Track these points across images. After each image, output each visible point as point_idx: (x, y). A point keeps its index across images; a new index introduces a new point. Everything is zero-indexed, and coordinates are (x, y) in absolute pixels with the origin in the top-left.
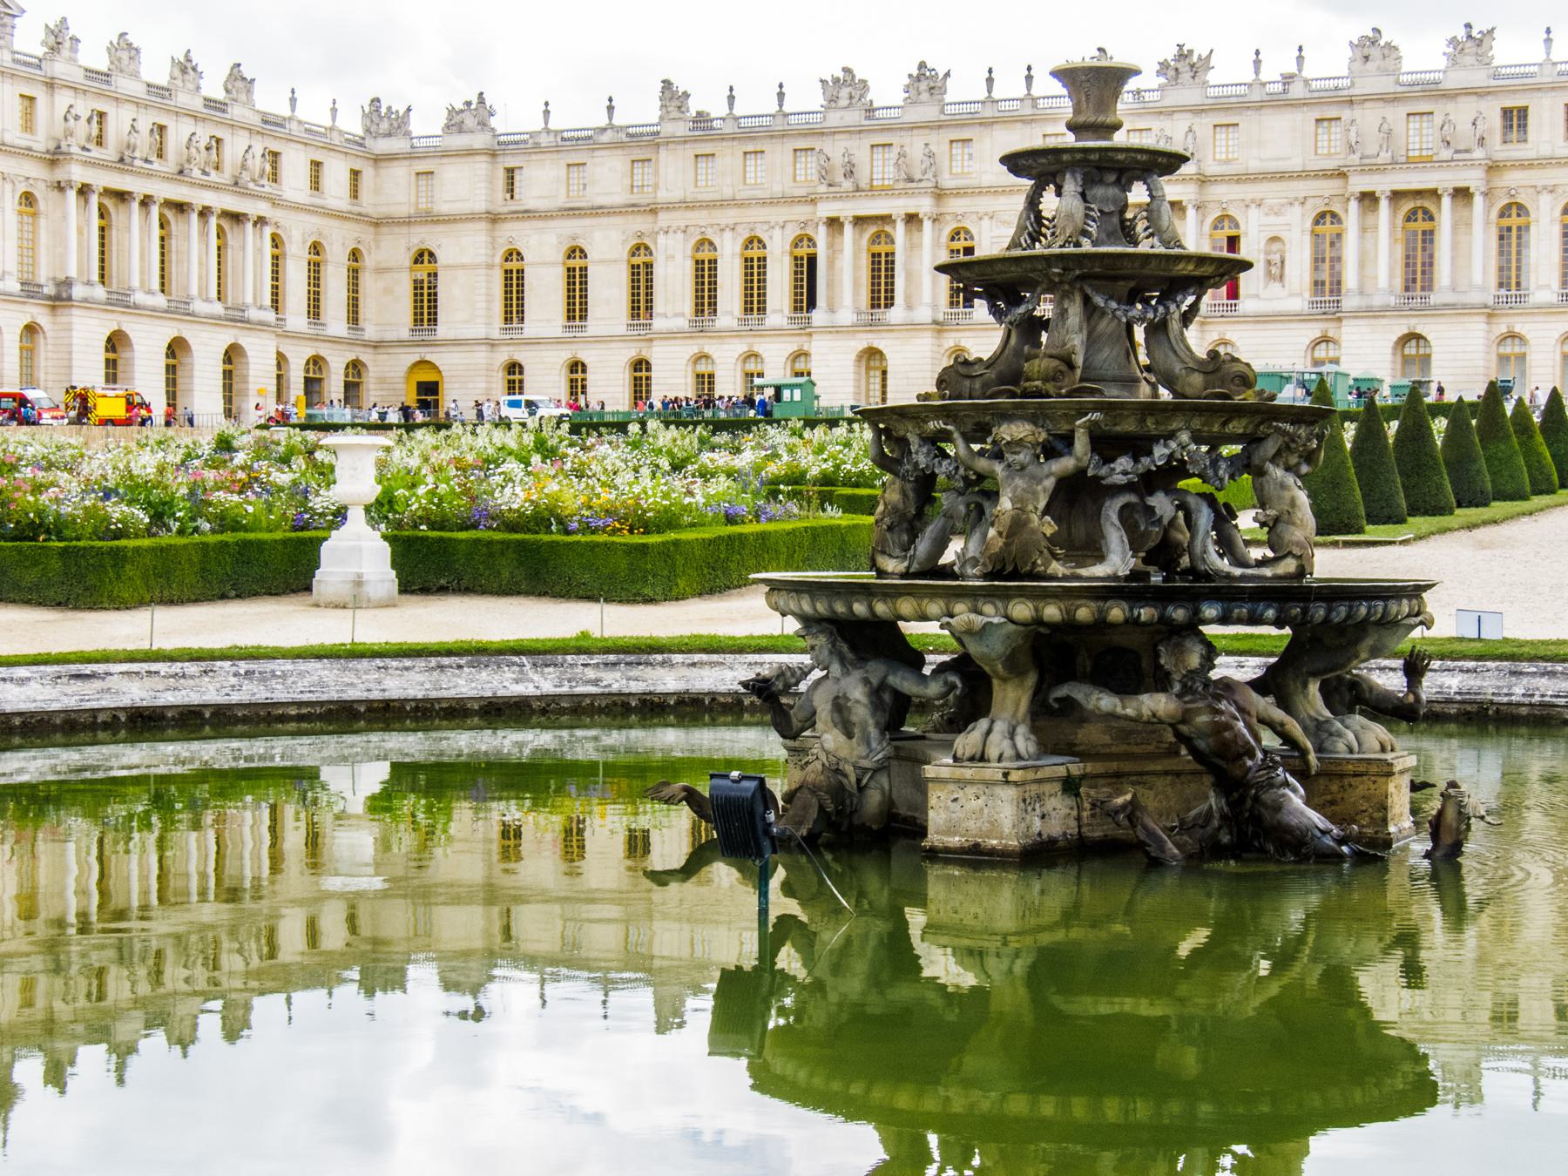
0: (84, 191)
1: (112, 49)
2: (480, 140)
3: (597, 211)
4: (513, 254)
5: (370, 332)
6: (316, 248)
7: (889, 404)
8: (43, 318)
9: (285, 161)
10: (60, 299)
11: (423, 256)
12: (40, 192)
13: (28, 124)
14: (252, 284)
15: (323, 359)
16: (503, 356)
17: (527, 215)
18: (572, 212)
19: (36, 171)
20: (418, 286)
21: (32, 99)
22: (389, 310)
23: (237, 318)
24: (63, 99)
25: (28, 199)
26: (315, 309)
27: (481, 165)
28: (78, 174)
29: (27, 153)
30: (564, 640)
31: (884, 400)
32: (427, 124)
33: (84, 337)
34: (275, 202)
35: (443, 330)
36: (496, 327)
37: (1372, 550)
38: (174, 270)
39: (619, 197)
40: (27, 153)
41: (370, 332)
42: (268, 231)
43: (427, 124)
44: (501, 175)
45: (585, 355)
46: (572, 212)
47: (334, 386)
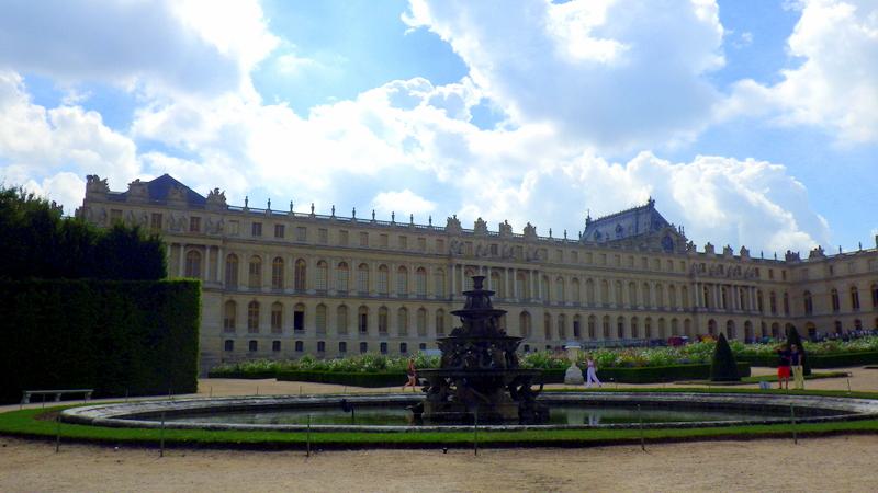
0: (699, 284)
1: (741, 252)
2: (820, 259)
3: (858, 276)
4: (835, 290)
5: (793, 315)
6: (773, 293)
7: (202, 293)
8: (690, 317)
9: (760, 271)
10: (695, 311)
11: (807, 293)
12: (688, 285)
13: (684, 268)
14: (752, 304)
15: (528, 313)
16: (834, 319)
17: (838, 278)
18: (851, 276)
19: (686, 280)
20: (806, 301)
21: (442, 241)
22: (797, 308)
23: (748, 313)
24: (692, 261)
25: (685, 287)
26: (774, 309)
27: (821, 266)
28: (697, 280)
29: (683, 275)
30: (241, 453)
31: (206, 290)
32: (804, 256)
33: (703, 320)
34: (759, 282)
35: (814, 313)
36: (831, 312)
37: (120, 429)
38: (728, 301)
39: (865, 271)
40: (683, 275)
41: (793, 315)
42: (756, 290)
43: (804, 256)
44: (828, 268)
45: (840, 319)
46: (851, 276)
47: (373, 321)
